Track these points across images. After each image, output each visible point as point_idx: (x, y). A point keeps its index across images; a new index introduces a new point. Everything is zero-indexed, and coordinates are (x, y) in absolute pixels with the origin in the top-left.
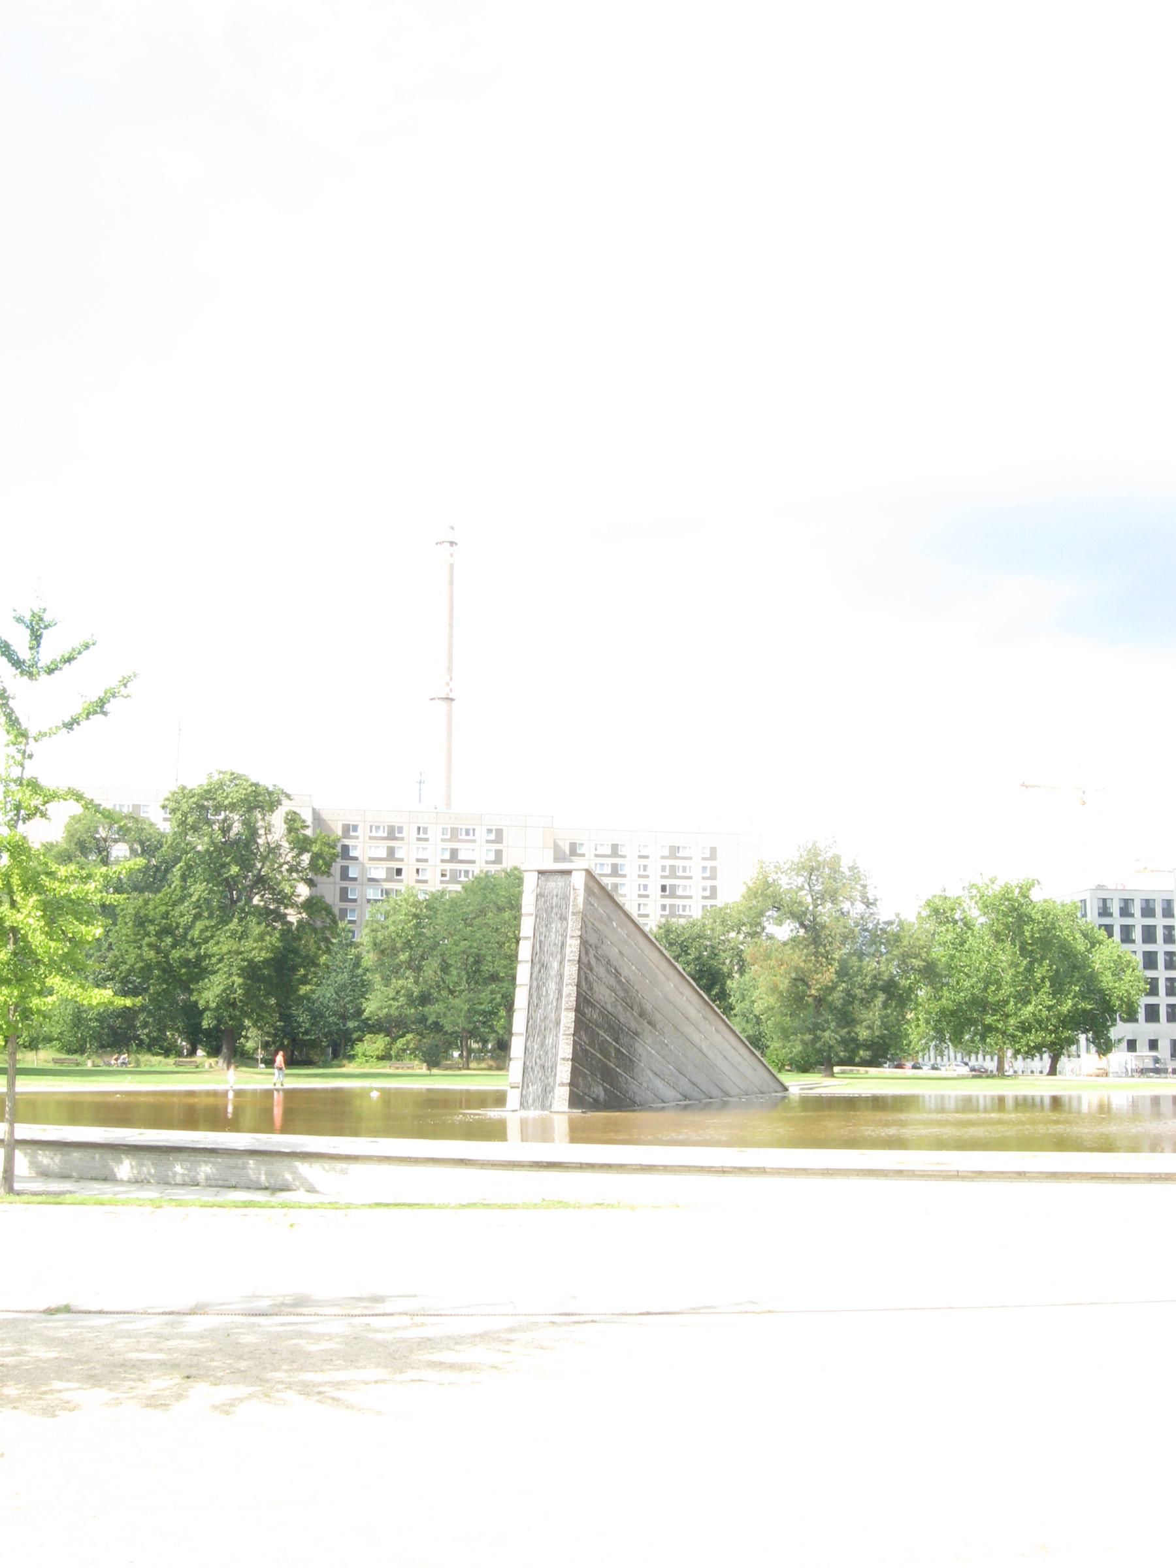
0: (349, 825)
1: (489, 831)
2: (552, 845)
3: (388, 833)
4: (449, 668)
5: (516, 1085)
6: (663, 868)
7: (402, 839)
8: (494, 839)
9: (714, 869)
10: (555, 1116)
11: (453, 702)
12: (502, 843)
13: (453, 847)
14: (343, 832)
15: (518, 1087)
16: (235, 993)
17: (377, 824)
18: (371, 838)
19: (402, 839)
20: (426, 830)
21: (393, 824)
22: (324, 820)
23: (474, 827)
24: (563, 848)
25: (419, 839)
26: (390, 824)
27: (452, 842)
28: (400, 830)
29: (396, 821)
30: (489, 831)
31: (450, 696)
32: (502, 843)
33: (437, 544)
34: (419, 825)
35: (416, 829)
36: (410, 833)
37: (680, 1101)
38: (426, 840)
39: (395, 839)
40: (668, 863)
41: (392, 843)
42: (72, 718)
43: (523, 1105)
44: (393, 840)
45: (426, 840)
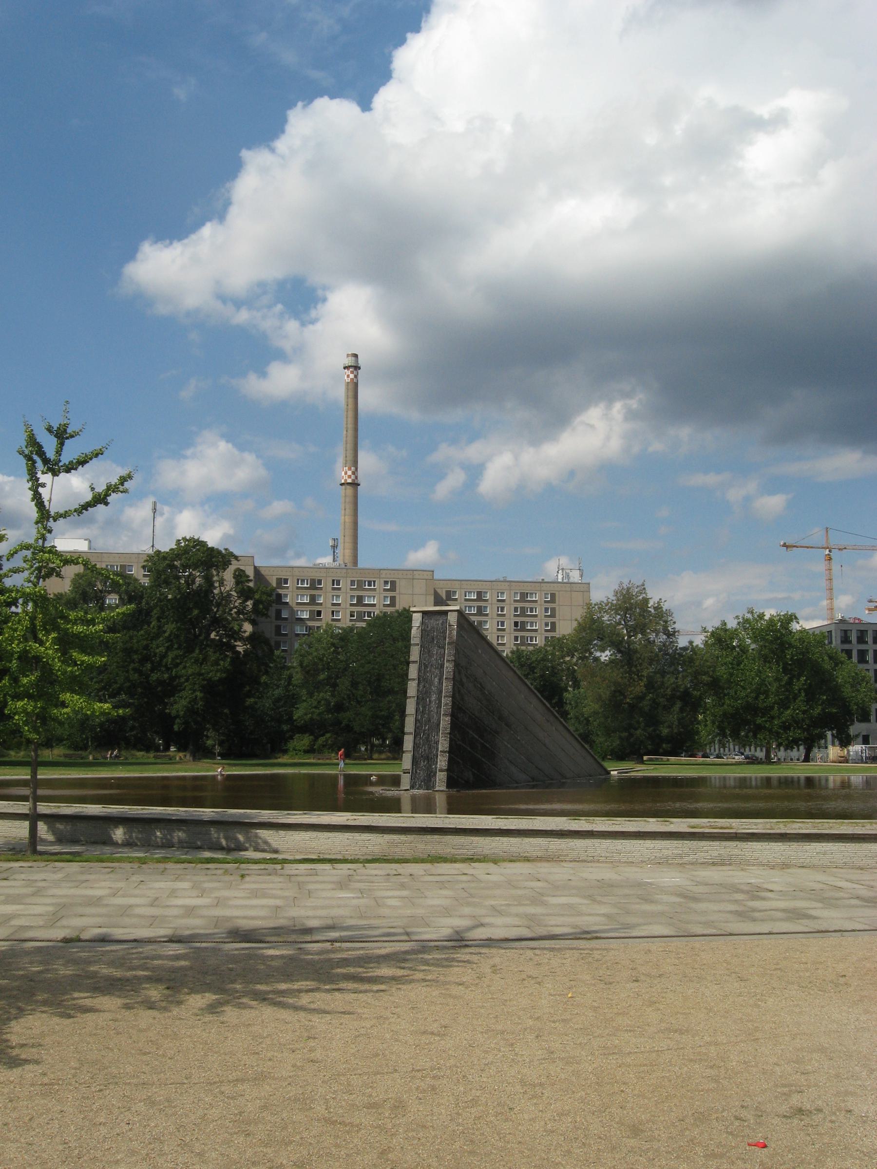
1: (386, 583)
6: (516, 609)
9: (553, 610)
12: (395, 591)
14: (277, 584)
20: (338, 583)
22: (262, 575)
23: (374, 580)
24: (441, 594)
25: (334, 589)
28: (320, 582)
29: (316, 575)
36: (326, 584)
38: (339, 589)
40: (519, 605)
42: (198, 539)
44: (314, 589)
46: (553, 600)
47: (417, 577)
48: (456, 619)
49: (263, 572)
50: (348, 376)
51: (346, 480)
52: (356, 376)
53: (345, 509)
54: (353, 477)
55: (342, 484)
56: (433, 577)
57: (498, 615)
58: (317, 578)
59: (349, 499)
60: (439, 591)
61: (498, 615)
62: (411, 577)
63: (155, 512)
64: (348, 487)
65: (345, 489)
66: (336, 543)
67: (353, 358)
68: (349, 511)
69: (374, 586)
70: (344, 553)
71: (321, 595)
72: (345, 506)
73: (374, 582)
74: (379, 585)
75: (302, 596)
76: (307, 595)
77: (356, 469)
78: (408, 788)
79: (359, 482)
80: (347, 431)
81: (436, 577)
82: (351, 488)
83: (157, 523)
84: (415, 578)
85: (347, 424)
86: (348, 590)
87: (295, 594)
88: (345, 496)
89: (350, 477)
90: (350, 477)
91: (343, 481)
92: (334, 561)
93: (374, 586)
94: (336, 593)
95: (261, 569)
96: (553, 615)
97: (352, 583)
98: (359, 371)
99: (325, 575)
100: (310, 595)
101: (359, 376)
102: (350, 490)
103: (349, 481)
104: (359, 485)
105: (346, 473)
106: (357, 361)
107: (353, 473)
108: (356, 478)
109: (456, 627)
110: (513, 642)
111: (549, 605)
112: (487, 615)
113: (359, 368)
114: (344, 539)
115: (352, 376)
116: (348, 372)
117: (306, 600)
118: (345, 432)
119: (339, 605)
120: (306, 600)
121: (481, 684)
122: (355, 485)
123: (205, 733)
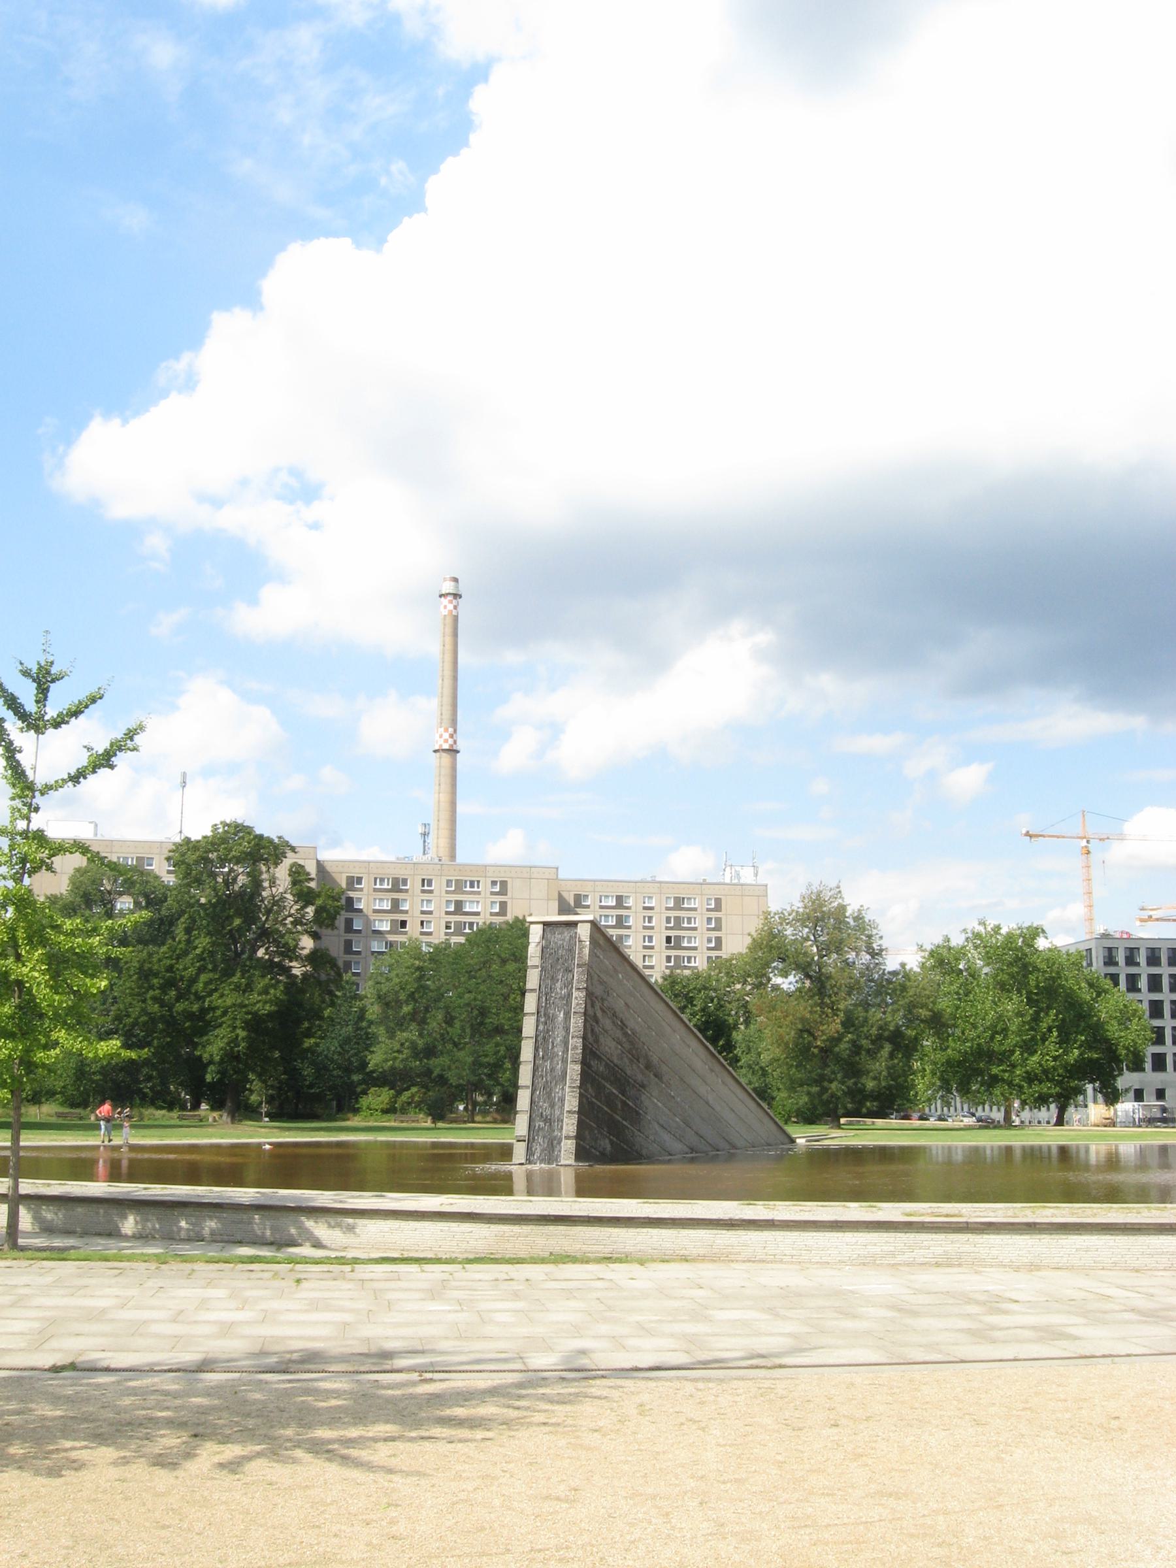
0: (580, 895)
1: (494, 883)
2: (557, 897)
4: (453, 720)
6: (668, 920)
9: (718, 920)
11: (458, 754)
15: (525, 1141)
17: (381, 876)
20: (430, 883)
22: (328, 872)
25: (423, 891)
28: (405, 882)
29: (400, 873)
30: (494, 883)
34: (424, 877)
36: (414, 885)
37: (687, 1153)
38: (431, 892)
39: (401, 891)
41: (396, 895)
44: (397, 892)
45: (431, 892)
46: (718, 908)
50: (445, 607)
51: (441, 745)
52: (455, 608)
53: (440, 785)
54: (451, 741)
55: (435, 751)
57: (645, 928)
59: (446, 771)
60: (565, 894)
61: (645, 928)
64: (444, 755)
66: (427, 830)
67: (453, 583)
69: (478, 887)
70: (437, 843)
74: (485, 887)
76: (388, 900)
77: (455, 731)
79: (458, 749)
81: (560, 876)
86: (444, 892)
91: (437, 748)
93: (478, 887)
94: (426, 896)
96: (718, 928)
97: (449, 883)
100: (392, 899)
103: (446, 746)
104: (458, 752)
105: (441, 736)
107: (451, 736)
108: (455, 742)
110: (443, 930)
111: (713, 915)
112: (629, 927)
114: (438, 825)
115: (451, 607)
116: (445, 601)
117: (386, 905)
119: (430, 913)
120: (386, 905)
122: (453, 752)
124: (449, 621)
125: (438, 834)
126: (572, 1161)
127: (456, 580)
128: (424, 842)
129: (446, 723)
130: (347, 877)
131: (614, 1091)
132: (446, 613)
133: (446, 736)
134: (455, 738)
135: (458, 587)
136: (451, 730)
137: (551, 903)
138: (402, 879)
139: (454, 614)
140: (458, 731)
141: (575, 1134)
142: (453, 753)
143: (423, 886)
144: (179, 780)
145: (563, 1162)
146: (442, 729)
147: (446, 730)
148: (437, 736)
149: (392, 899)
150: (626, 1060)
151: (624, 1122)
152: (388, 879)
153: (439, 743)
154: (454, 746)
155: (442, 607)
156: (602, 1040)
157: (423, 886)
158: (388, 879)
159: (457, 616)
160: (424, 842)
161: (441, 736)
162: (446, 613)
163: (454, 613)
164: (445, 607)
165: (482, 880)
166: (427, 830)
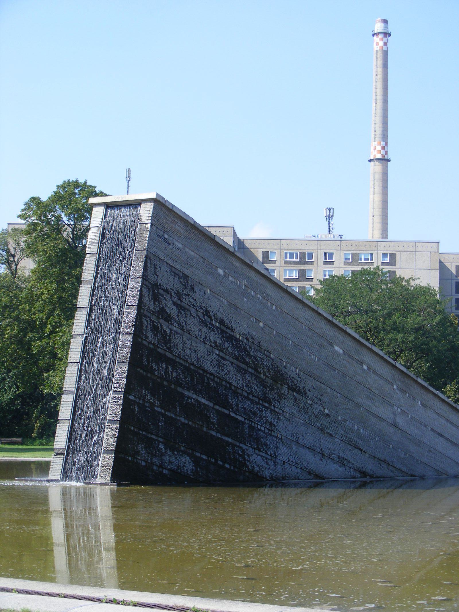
1: (385, 256)
2: (437, 266)
3: (300, 259)
4: (384, 135)
5: (61, 451)
7: (312, 263)
8: (388, 261)
10: (98, 488)
11: (389, 163)
12: (395, 265)
13: (354, 269)
14: (263, 258)
15: (63, 454)
16: (292, 413)
17: (290, 251)
18: (286, 262)
19: (312, 263)
20: (331, 256)
21: (304, 251)
22: (248, 248)
24: (451, 269)
25: (326, 263)
26: (301, 251)
27: (353, 265)
28: (310, 255)
29: (307, 248)
30: (385, 256)
31: (386, 157)
32: (395, 265)
33: (373, 35)
34: (326, 251)
35: (324, 254)
36: (318, 258)
41: (303, 267)
42: (86, 183)
43: (66, 474)
44: (304, 264)
45: (332, 263)
47: (420, 249)
48: (151, 212)
49: (248, 245)
50: (377, 44)
51: (375, 156)
52: (385, 44)
53: (374, 187)
54: (383, 152)
56: (438, 249)
58: (307, 252)
59: (378, 176)
60: (449, 266)
62: (411, 249)
63: (129, 180)
64: (377, 163)
65: (374, 166)
66: (331, 214)
67: (383, 24)
68: (378, 189)
70: (373, 234)
71: (312, 270)
72: (374, 184)
73: (372, 255)
75: (291, 271)
76: (296, 270)
77: (386, 144)
78: (59, 478)
79: (389, 158)
80: (376, 103)
81: (441, 251)
82: (380, 163)
83: (431, 273)
84: (417, 250)
85: (376, 96)
86: (342, 263)
87: (282, 269)
88: (374, 173)
89: (379, 152)
90: (379, 152)
91: (372, 158)
92: (329, 232)
95: (245, 242)
98: (389, 38)
99: (316, 248)
100: (300, 270)
101: (389, 45)
102: (378, 167)
103: (379, 156)
105: (375, 149)
106: (386, 27)
107: (383, 148)
108: (386, 153)
109: (149, 225)
113: (390, 35)
114: (373, 219)
115: (381, 43)
116: (376, 39)
117: (295, 275)
118: (374, 104)
120: (295, 275)
121: (222, 322)
122: (385, 160)
123: (27, 411)
124: (380, 54)
125: (373, 227)
126: (107, 480)
127: (385, 22)
128: (329, 223)
129: (379, 137)
130: (263, 252)
131: (203, 401)
132: (378, 49)
133: (379, 148)
134: (386, 150)
135: (387, 28)
136: (383, 143)
137: (433, 272)
138: (308, 253)
139: (384, 49)
140: (389, 144)
141: (114, 447)
142: (384, 162)
143: (286, 258)
144: (125, 174)
145: (98, 480)
146: (376, 143)
147: (379, 144)
148: (372, 148)
149: (300, 270)
150: (229, 367)
151: (225, 438)
152: (296, 254)
153: (374, 154)
154: (386, 156)
155: (375, 44)
156: (176, 340)
157: (326, 259)
158: (296, 254)
159: (387, 51)
160: (329, 223)
161: (375, 149)
162: (378, 49)
163: (385, 48)
164: (377, 44)
165: (375, 253)
166: (331, 214)
